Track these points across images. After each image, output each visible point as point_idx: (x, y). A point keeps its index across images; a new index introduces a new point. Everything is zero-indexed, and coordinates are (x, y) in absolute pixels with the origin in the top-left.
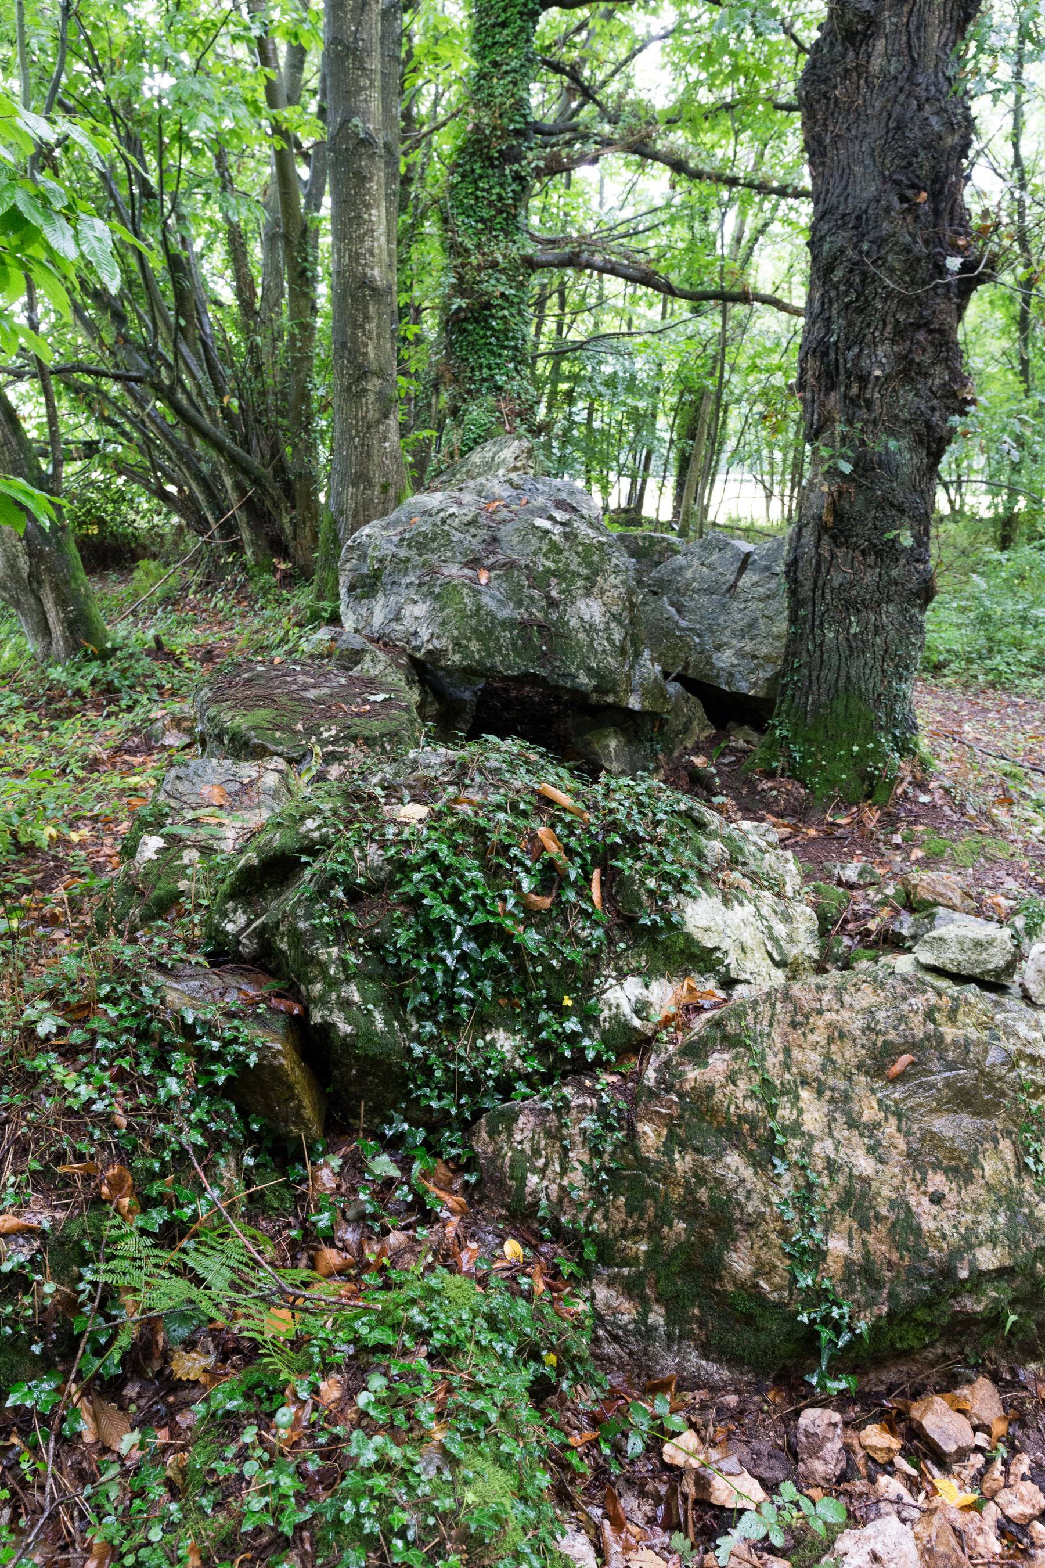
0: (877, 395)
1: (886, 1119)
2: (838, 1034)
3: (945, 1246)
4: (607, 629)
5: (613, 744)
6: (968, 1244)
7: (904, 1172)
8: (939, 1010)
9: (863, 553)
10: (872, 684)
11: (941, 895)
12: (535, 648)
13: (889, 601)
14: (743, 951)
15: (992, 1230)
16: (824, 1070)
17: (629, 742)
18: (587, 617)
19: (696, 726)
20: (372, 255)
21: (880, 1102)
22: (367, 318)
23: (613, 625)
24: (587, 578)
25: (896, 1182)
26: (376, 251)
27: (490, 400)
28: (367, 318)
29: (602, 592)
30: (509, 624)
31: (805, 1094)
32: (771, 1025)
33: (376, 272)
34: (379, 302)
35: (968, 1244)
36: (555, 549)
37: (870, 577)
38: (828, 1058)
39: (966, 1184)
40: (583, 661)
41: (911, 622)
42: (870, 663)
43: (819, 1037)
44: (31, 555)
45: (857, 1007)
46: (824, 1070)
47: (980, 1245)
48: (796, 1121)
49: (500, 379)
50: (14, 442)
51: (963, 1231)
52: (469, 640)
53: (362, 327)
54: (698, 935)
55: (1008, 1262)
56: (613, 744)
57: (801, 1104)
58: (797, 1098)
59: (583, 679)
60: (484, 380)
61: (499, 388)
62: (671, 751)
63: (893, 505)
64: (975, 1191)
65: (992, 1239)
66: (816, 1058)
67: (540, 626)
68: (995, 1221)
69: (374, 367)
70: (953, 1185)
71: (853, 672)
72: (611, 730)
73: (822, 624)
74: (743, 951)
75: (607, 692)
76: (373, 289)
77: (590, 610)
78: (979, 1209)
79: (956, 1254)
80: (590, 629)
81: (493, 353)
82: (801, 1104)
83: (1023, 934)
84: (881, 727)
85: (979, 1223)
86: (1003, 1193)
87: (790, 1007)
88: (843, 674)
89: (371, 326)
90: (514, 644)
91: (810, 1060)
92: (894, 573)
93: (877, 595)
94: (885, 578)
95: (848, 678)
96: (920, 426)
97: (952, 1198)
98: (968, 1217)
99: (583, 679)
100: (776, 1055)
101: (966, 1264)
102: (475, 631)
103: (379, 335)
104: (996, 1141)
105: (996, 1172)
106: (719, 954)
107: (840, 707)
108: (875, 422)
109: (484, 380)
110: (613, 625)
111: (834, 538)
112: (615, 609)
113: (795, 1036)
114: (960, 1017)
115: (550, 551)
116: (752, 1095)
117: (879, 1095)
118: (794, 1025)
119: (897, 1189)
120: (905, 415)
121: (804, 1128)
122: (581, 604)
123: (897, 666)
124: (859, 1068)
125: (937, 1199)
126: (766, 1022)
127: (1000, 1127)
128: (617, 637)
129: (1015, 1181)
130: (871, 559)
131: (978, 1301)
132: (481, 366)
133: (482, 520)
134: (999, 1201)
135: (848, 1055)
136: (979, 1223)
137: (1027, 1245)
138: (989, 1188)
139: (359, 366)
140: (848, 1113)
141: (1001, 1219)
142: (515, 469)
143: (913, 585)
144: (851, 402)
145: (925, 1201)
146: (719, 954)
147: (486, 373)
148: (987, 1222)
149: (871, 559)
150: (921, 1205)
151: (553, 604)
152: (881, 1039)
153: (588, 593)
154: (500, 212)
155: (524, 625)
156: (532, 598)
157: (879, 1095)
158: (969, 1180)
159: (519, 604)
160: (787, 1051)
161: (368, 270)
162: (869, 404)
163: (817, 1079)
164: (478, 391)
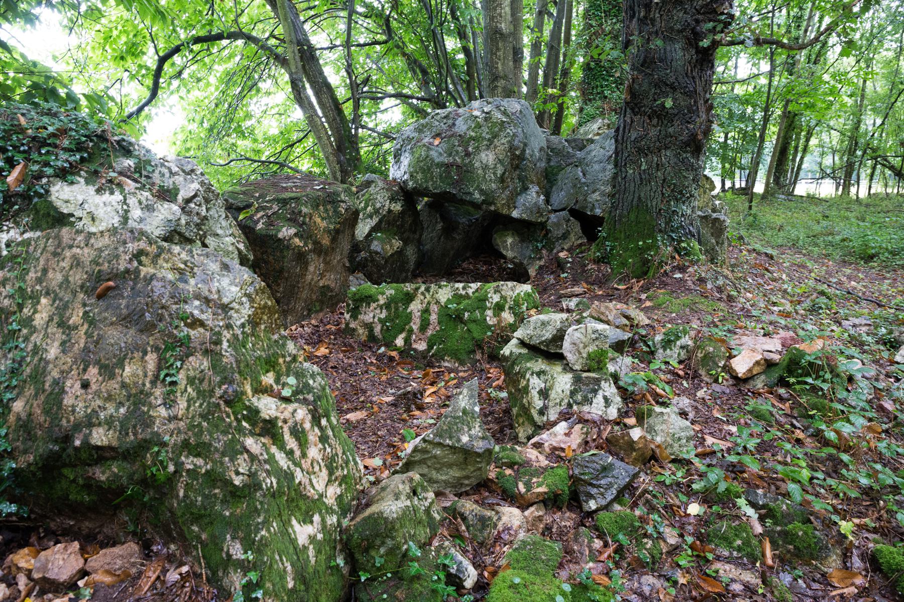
0: (657, 15)
1: (83, 325)
2: (77, 263)
3: (72, 419)
4: (495, 167)
5: (510, 241)
6: (90, 422)
7: (75, 363)
8: (147, 255)
9: (650, 118)
10: (656, 203)
11: (603, 314)
12: (452, 177)
13: (666, 148)
14: (93, 219)
15: (111, 416)
16: (60, 286)
17: (522, 241)
18: (484, 162)
19: (572, 237)
20: (501, 17)
21: (86, 313)
22: (498, 49)
23: (498, 165)
24: (489, 140)
25: (65, 367)
26: (503, 15)
27: (599, 103)
28: (498, 49)
29: (495, 147)
30: (440, 165)
31: (44, 301)
32: (42, 254)
33: (503, 25)
34: (504, 41)
35: (90, 422)
36: (479, 126)
37: (653, 132)
38: (66, 280)
39: (109, 379)
40: (478, 186)
41: (683, 162)
42: (654, 189)
43: (65, 264)
44: (342, 172)
45: (96, 247)
46: (60, 286)
47: (99, 425)
48: (30, 317)
49: (607, 93)
50: (338, 119)
51: (89, 411)
52: (417, 173)
53: (495, 54)
54: (58, 204)
55: (115, 443)
56: (510, 241)
57: (39, 307)
58: (38, 302)
59: (477, 195)
60: (598, 93)
61: (606, 97)
62: (552, 250)
63: (667, 85)
64: (114, 385)
65: (109, 423)
66: (59, 277)
67: (458, 166)
68: (117, 410)
69: (502, 74)
70: (100, 379)
71: (642, 195)
72: (510, 233)
73: (625, 164)
74: (93, 219)
75: (490, 204)
76: (501, 34)
77: (488, 157)
78: (109, 398)
79: (77, 427)
80: (485, 168)
81: (604, 79)
82: (39, 307)
83: (659, 346)
84: (660, 231)
85: (105, 409)
86: (134, 391)
87: (56, 243)
88: (637, 195)
89: (500, 53)
90: (441, 176)
91: (55, 277)
92: (671, 130)
93: (658, 144)
94: (663, 133)
95: (639, 198)
96: (688, 33)
97: (94, 387)
98: (99, 402)
99: (477, 195)
100: (36, 272)
101: (81, 436)
102: (421, 168)
103: (504, 58)
104: (145, 353)
105: (134, 375)
106: (72, 219)
107: (633, 217)
108: (657, 33)
109: (598, 93)
110: (498, 165)
111: (632, 109)
112: (501, 157)
113: (53, 263)
114: (160, 261)
115: (475, 127)
116: (11, 296)
117: (87, 309)
118: (55, 254)
119: (62, 372)
120: (678, 27)
121: (34, 323)
122: (483, 155)
123: (672, 191)
124: (82, 287)
125: (85, 385)
126: (39, 251)
127: (151, 343)
128: (499, 173)
129: (148, 385)
130: (655, 121)
131: (103, 473)
132: (597, 86)
133: (451, 116)
134: (129, 397)
135: (78, 277)
136: (105, 409)
137: (135, 434)
138: (124, 385)
139: (493, 74)
140: (61, 316)
141: (122, 410)
142: (598, 134)
143: (684, 137)
144: (642, 21)
145: (78, 385)
146: (72, 219)
147: (599, 89)
148: (111, 409)
149: (655, 121)
150: (73, 387)
151: (468, 154)
152: (98, 268)
153: (488, 148)
154: (614, 7)
155: (448, 166)
156: (457, 152)
157: (87, 309)
158: (112, 376)
159: (450, 155)
160: (45, 271)
161: (498, 24)
162: (653, 21)
163: (54, 292)
164: (594, 99)
